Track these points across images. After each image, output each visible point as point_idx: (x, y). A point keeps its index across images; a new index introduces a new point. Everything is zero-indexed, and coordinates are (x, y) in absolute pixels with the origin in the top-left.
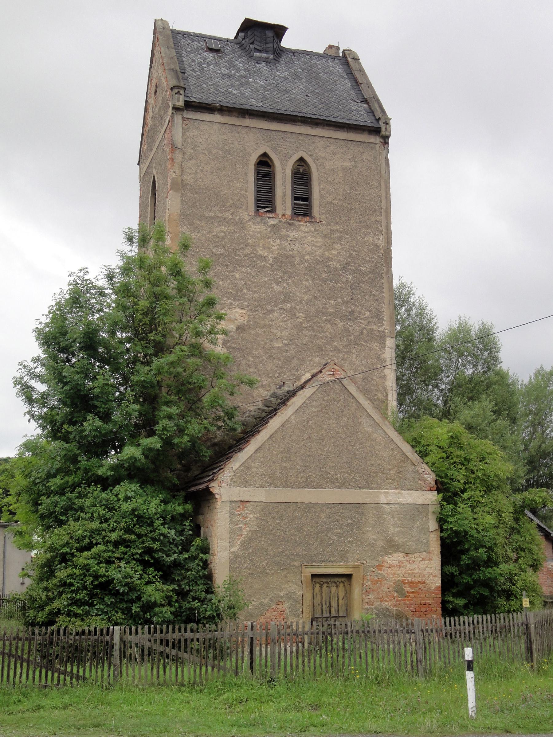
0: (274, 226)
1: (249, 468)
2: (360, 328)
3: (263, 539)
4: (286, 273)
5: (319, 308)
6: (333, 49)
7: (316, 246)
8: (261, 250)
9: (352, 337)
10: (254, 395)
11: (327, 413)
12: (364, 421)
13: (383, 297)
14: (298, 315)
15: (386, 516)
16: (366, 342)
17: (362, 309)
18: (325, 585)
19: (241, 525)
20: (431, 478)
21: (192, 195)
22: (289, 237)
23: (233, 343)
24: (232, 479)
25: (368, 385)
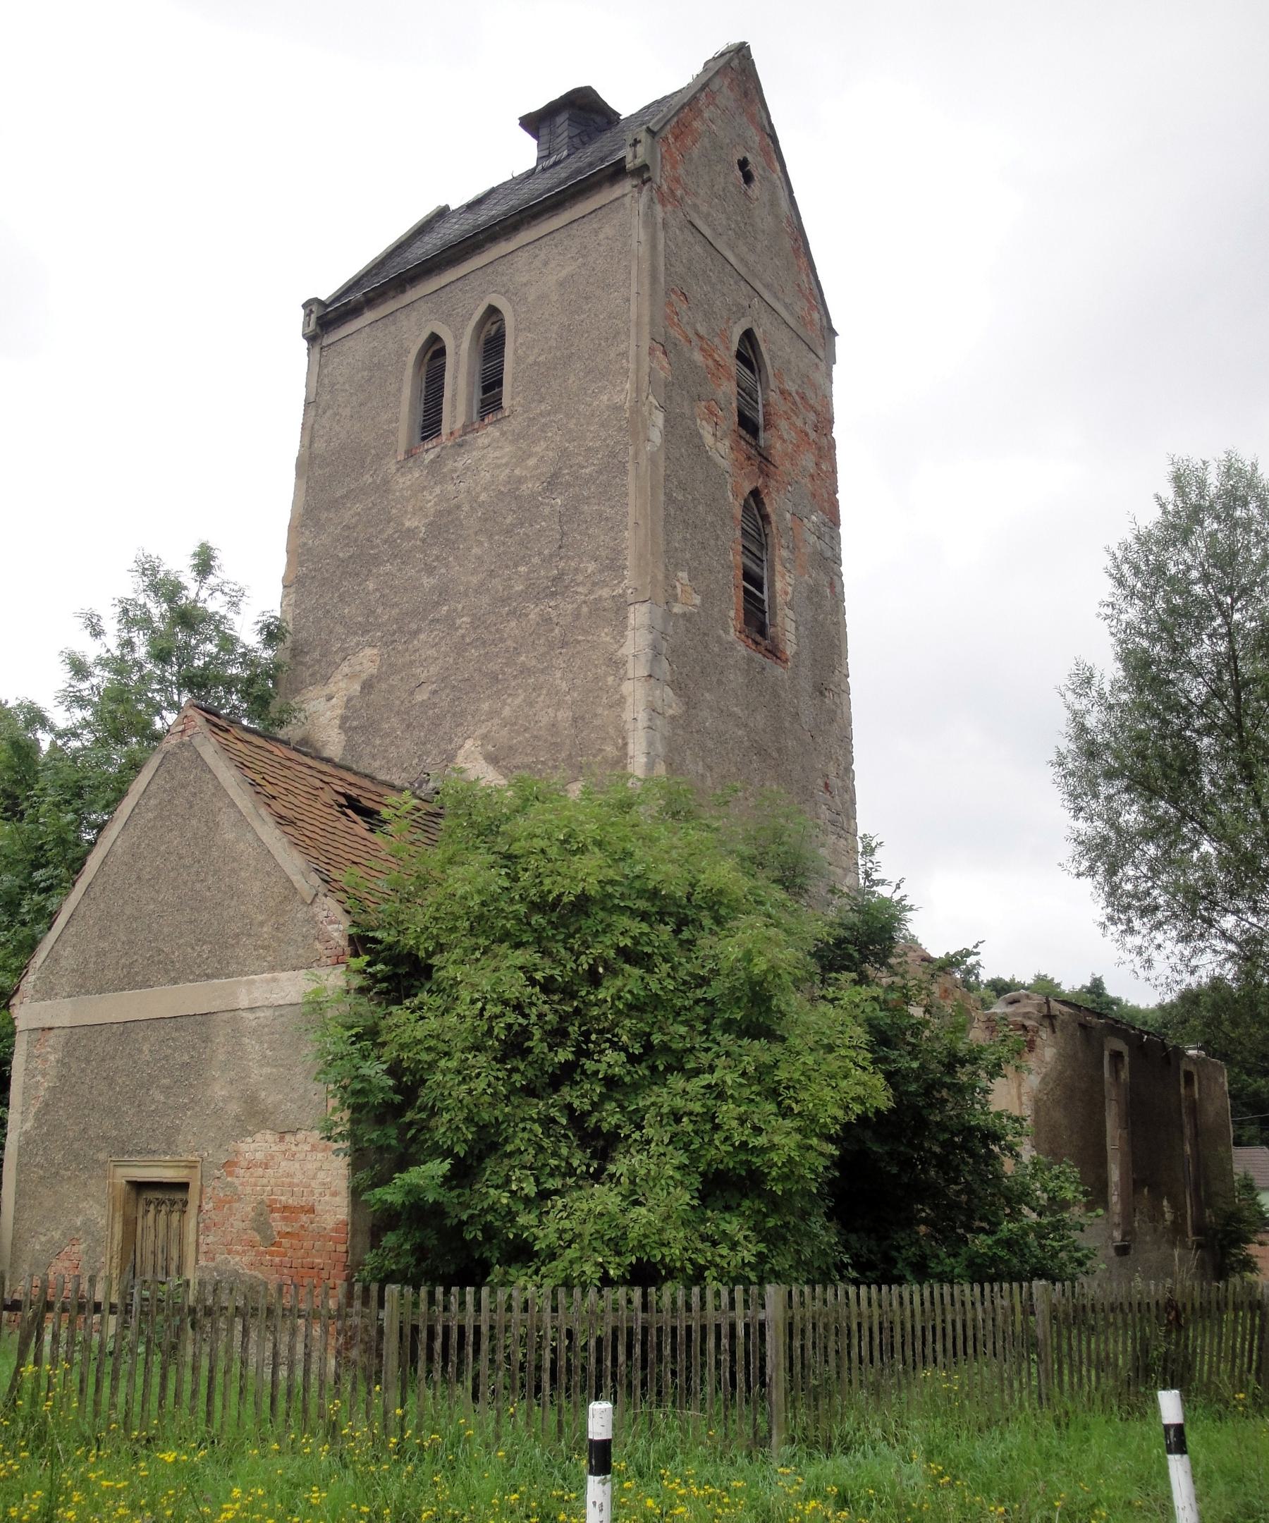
2: (575, 606)
12: (226, 818)
13: (625, 515)
14: (458, 622)
16: (585, 632)
17: (581, 561)
20: (339, 930)
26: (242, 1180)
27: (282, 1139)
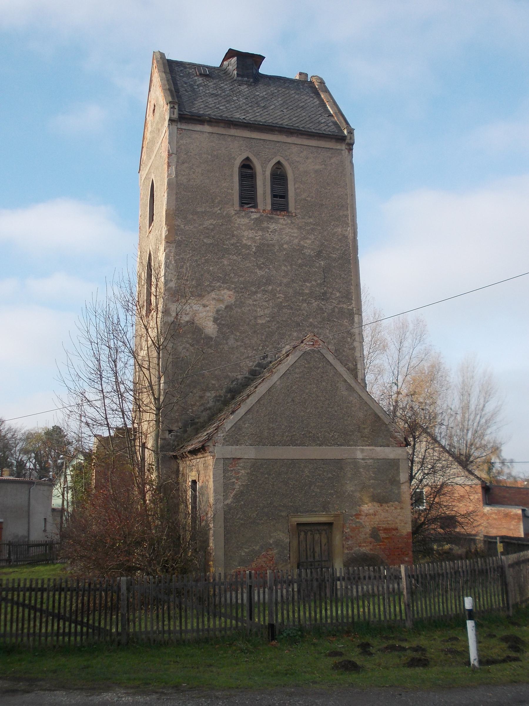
0: (256, 219)
1: (240, 429)
3: (254, 492)
4: (267, 260)
5: (296, 289)
6: (303, 76)
7: (293, 237)
8: (246, 240)
9: (326, 314)
10: (242, 366)
11: (308, 379)
13: (351, 280)
14: (278, 295)
15: (362, 470)
16: (337, 318)
18: (309, 533)
19: (234, 480)
21: (185, 193)
22: (269, 228)
23: (222, 320)
24: (224, 439)
25: (340, 356)
26: (363, 519)
27: (381, 506)
